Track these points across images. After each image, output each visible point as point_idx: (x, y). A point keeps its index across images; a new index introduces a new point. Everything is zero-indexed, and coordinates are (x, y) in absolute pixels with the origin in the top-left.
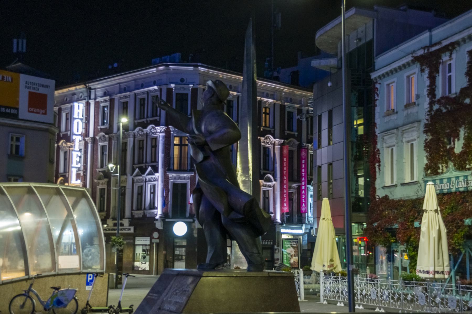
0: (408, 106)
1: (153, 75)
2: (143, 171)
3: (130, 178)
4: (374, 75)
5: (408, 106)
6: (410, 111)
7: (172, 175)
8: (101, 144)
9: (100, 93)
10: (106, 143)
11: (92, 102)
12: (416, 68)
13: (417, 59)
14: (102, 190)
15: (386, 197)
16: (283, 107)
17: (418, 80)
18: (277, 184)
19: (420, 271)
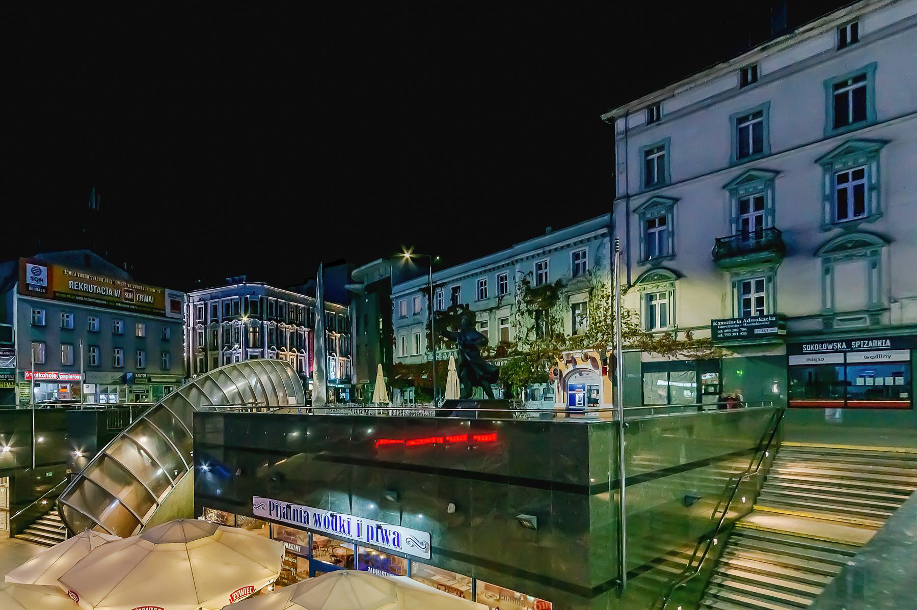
0: (415, 314)
1: (234, 289)
2: (230, 348)
3: (221, 353)
4: (391, 297)
5: (415, 314)
6: (416, 317)
7: (248, 350)
8: (198, 331)
9: (196, 299)
10: (203, 331)
11: (191, 305)
12: (420, 295)
13: (421, 290)
14: (201, 360)
15: (400, 363)
16: (309, 309)
17: (420, 302)
18: (306, 355)
19: (781, 344)
